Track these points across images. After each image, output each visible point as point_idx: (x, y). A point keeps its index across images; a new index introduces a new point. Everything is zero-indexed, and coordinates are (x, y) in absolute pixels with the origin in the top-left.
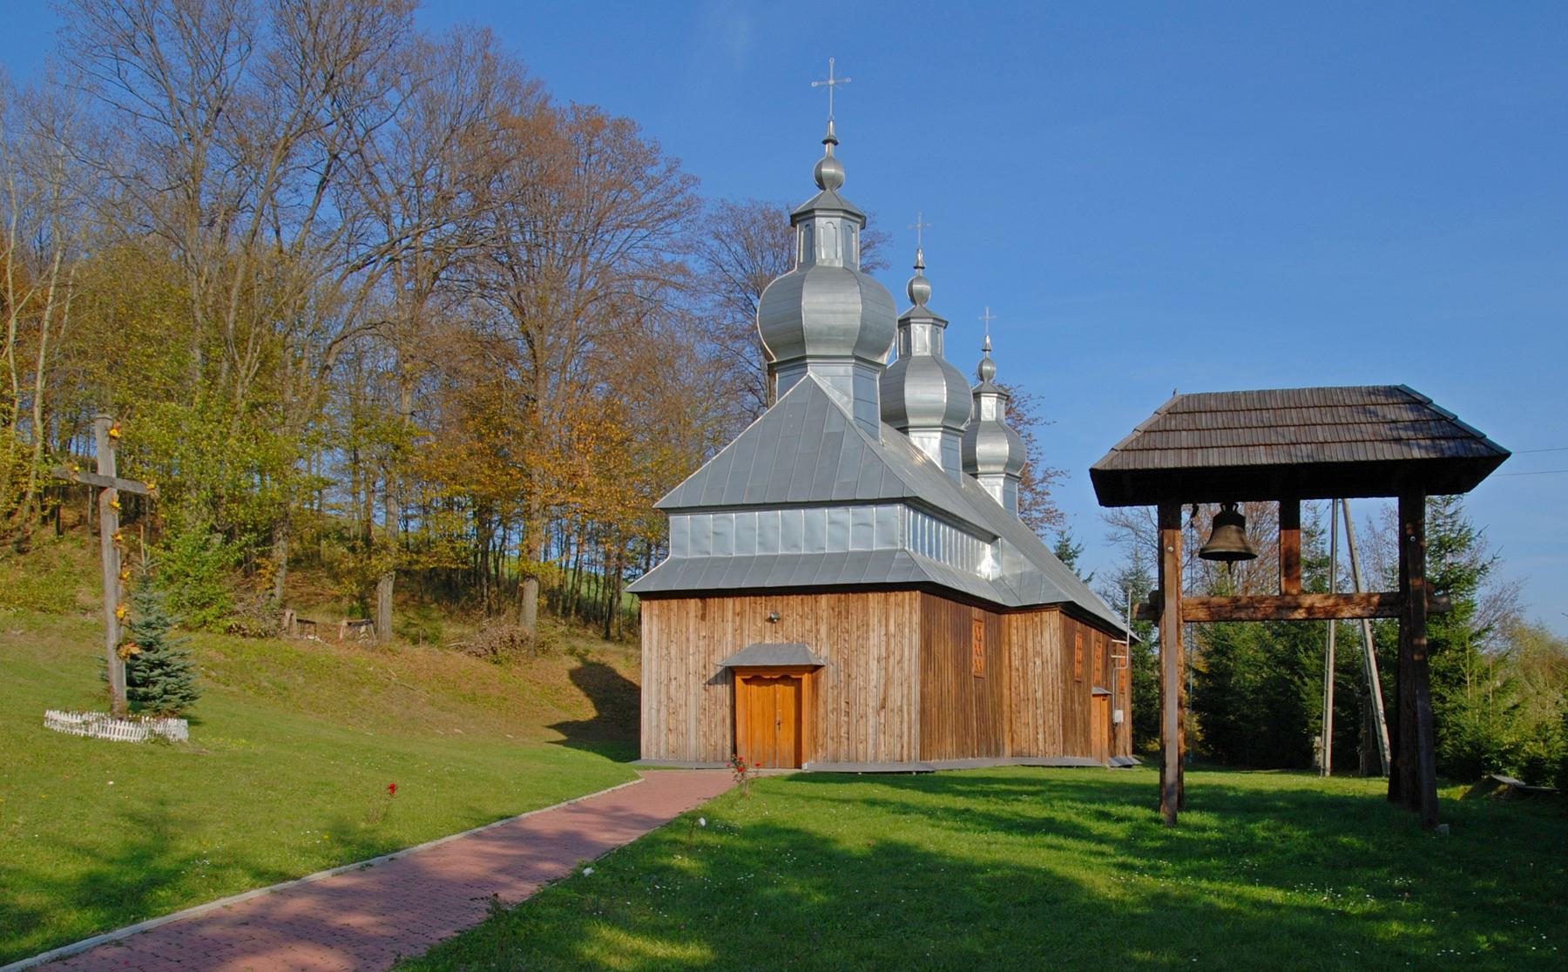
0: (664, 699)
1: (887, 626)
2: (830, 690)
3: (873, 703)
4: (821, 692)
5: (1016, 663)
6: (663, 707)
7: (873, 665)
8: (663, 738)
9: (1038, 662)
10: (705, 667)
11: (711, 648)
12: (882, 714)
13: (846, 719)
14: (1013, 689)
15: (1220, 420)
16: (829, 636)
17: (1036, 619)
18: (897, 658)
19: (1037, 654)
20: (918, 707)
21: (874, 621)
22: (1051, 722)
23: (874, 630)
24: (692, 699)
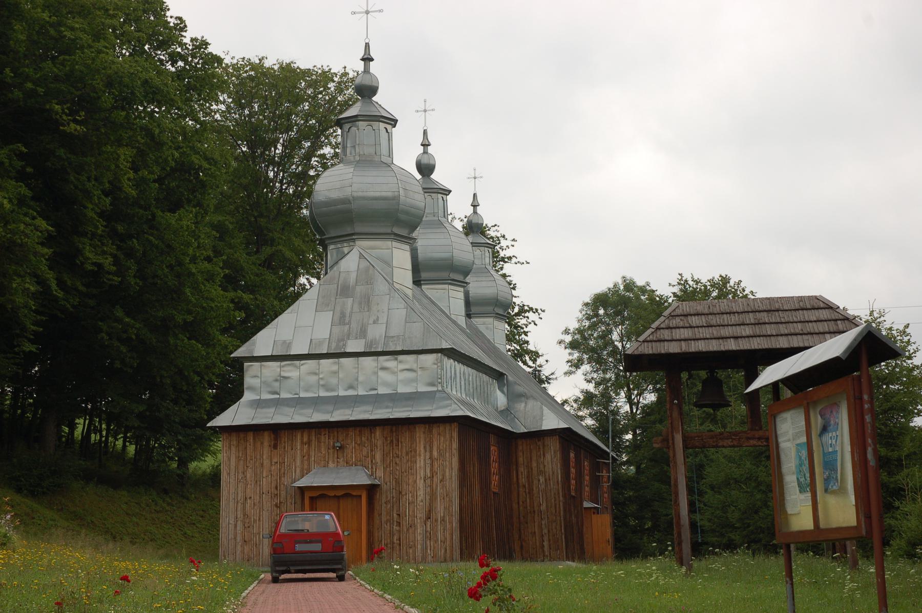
0: (240, 514)
1: (431, 451)
2: (384, 505)
3: (421, 514)
4: (377, 507)
5: (523, 480)
6: (239, 522)
7: (420, 484)
8: (239, 548)
9: (542, 479)
10: (276, 488)
11: (282, 471)
12: (429, 523)
13: (398, 528)
14: (521, 503)
15: (704, 320)
16: (383, 460)
17: (540, 443)
18: (440, 477)
19: (541, 472)
20: (457, 516)
21: (421, 448)
22: (554, 530)
23: (420, 455)
24: (265, 514)
